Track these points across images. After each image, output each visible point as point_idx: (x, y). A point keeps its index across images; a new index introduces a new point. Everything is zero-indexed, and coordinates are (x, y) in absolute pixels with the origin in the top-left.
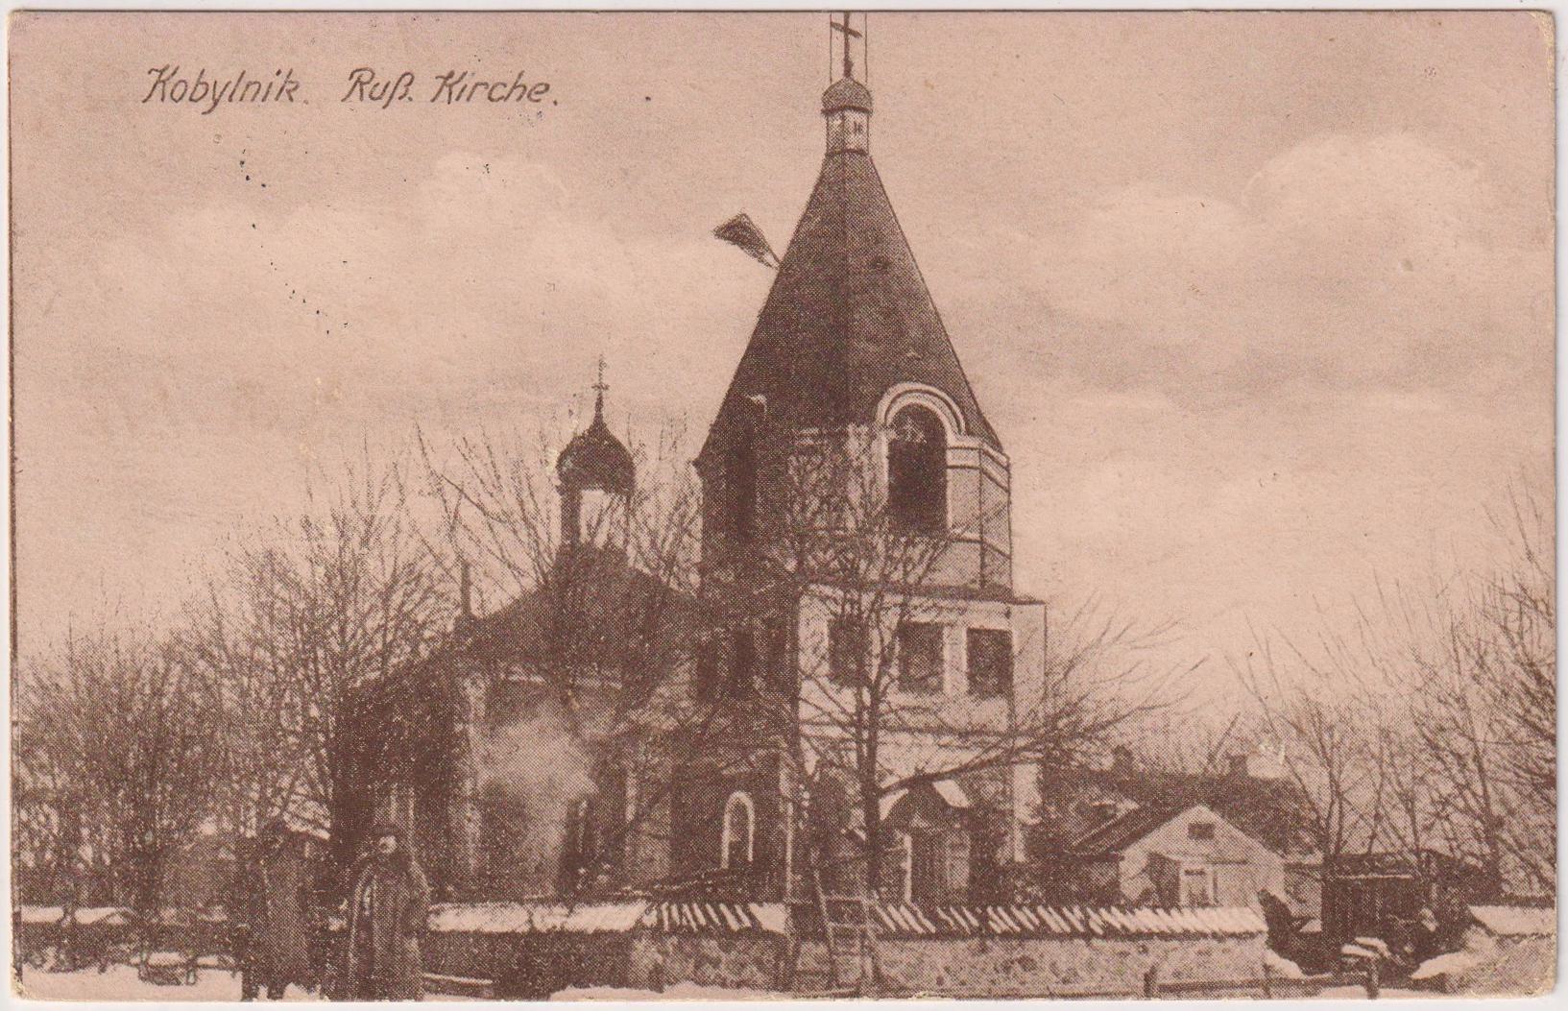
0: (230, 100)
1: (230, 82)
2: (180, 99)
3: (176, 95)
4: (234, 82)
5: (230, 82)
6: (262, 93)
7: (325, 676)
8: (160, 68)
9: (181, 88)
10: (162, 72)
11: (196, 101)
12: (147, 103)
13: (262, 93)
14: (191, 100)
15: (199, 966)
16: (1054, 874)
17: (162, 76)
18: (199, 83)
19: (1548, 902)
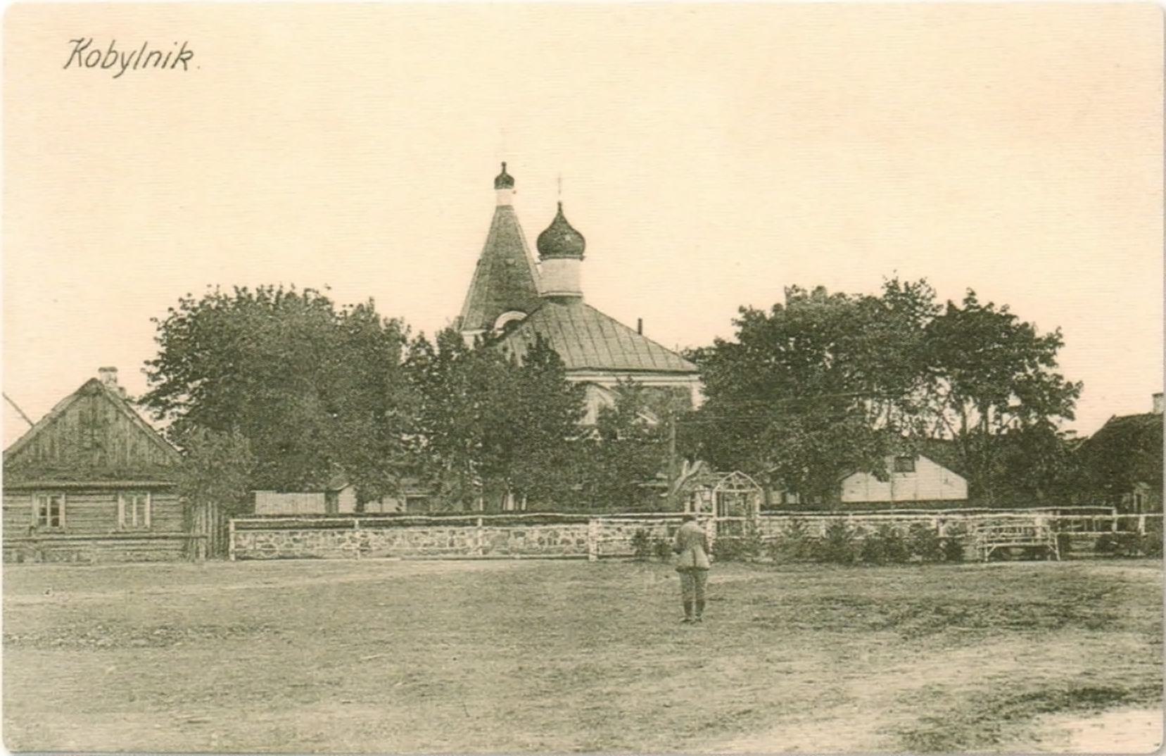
0: (135, 68)
1: (135, 52)
2: (94, 65)
3: (91, 62)
4: (138, 52)
5: (135, 52)
6: (163, 60)
7: (355, 381)
8: (79, 39)
9: (95, 56)
10: (80, 42)
11: (108, 67)
12: (118, 79)
13: (163, 60)
14: (103, 66)
15: (32, 424)
16: (305, 476)
17: (80, 46)
18: (110, 52)
19: (4, 547)
